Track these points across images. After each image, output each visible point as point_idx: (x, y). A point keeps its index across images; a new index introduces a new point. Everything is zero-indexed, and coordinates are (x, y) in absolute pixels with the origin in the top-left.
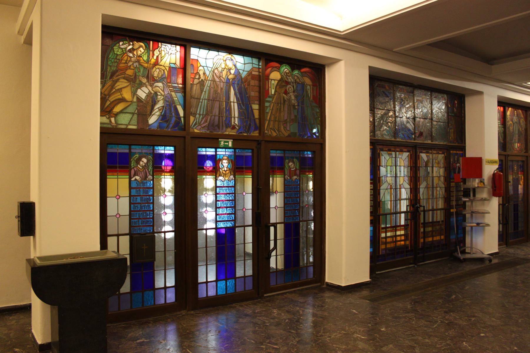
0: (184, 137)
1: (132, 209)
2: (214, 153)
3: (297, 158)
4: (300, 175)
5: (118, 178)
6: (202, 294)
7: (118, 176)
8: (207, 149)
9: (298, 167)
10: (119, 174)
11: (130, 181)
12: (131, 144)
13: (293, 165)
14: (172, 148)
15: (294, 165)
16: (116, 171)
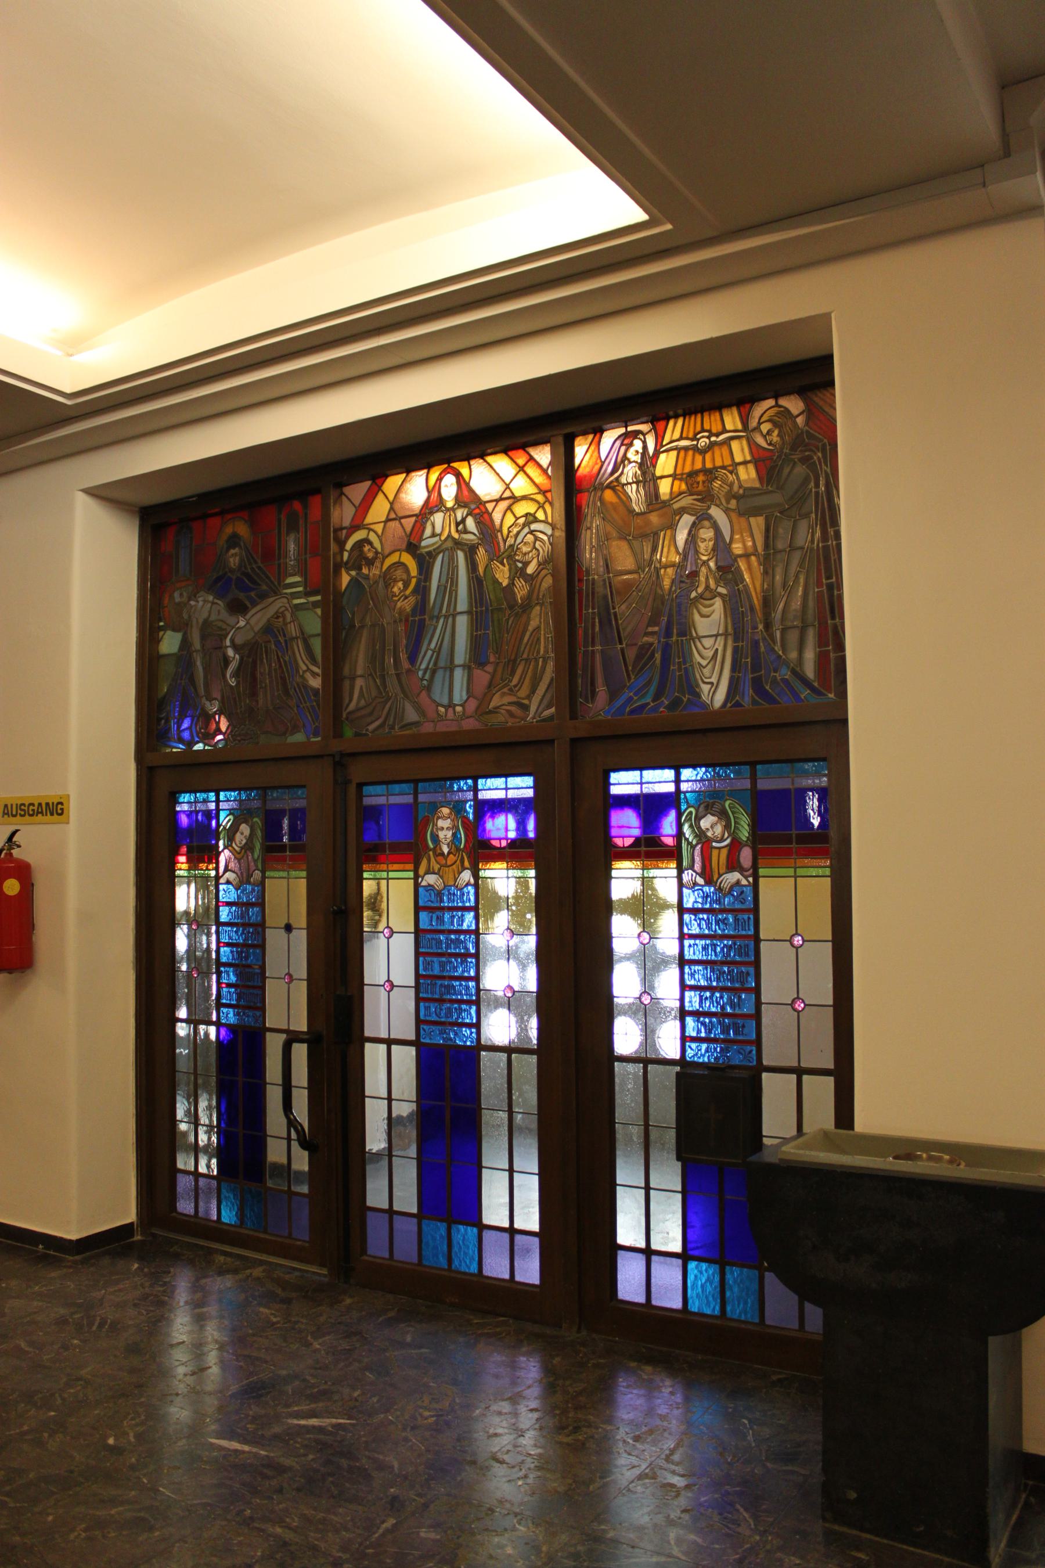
0: (574, 741)
1: (421, 972)
2: (670, 788)
3: (733, 794)
4: (755, 867)
5: (796, 877)
6: (377, 1246)
7: (795, 868)
8: (645, 773)
9: (744, 834)
10: (799, 862)
11: (417, 886)
12: (419, 777)
13: (718, 829)
14: (529, 781)
15: (727, 827)
16: (788, 853)
